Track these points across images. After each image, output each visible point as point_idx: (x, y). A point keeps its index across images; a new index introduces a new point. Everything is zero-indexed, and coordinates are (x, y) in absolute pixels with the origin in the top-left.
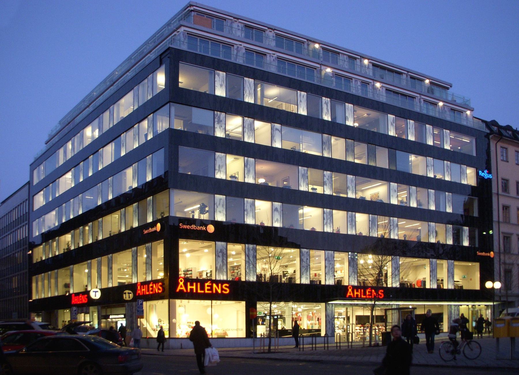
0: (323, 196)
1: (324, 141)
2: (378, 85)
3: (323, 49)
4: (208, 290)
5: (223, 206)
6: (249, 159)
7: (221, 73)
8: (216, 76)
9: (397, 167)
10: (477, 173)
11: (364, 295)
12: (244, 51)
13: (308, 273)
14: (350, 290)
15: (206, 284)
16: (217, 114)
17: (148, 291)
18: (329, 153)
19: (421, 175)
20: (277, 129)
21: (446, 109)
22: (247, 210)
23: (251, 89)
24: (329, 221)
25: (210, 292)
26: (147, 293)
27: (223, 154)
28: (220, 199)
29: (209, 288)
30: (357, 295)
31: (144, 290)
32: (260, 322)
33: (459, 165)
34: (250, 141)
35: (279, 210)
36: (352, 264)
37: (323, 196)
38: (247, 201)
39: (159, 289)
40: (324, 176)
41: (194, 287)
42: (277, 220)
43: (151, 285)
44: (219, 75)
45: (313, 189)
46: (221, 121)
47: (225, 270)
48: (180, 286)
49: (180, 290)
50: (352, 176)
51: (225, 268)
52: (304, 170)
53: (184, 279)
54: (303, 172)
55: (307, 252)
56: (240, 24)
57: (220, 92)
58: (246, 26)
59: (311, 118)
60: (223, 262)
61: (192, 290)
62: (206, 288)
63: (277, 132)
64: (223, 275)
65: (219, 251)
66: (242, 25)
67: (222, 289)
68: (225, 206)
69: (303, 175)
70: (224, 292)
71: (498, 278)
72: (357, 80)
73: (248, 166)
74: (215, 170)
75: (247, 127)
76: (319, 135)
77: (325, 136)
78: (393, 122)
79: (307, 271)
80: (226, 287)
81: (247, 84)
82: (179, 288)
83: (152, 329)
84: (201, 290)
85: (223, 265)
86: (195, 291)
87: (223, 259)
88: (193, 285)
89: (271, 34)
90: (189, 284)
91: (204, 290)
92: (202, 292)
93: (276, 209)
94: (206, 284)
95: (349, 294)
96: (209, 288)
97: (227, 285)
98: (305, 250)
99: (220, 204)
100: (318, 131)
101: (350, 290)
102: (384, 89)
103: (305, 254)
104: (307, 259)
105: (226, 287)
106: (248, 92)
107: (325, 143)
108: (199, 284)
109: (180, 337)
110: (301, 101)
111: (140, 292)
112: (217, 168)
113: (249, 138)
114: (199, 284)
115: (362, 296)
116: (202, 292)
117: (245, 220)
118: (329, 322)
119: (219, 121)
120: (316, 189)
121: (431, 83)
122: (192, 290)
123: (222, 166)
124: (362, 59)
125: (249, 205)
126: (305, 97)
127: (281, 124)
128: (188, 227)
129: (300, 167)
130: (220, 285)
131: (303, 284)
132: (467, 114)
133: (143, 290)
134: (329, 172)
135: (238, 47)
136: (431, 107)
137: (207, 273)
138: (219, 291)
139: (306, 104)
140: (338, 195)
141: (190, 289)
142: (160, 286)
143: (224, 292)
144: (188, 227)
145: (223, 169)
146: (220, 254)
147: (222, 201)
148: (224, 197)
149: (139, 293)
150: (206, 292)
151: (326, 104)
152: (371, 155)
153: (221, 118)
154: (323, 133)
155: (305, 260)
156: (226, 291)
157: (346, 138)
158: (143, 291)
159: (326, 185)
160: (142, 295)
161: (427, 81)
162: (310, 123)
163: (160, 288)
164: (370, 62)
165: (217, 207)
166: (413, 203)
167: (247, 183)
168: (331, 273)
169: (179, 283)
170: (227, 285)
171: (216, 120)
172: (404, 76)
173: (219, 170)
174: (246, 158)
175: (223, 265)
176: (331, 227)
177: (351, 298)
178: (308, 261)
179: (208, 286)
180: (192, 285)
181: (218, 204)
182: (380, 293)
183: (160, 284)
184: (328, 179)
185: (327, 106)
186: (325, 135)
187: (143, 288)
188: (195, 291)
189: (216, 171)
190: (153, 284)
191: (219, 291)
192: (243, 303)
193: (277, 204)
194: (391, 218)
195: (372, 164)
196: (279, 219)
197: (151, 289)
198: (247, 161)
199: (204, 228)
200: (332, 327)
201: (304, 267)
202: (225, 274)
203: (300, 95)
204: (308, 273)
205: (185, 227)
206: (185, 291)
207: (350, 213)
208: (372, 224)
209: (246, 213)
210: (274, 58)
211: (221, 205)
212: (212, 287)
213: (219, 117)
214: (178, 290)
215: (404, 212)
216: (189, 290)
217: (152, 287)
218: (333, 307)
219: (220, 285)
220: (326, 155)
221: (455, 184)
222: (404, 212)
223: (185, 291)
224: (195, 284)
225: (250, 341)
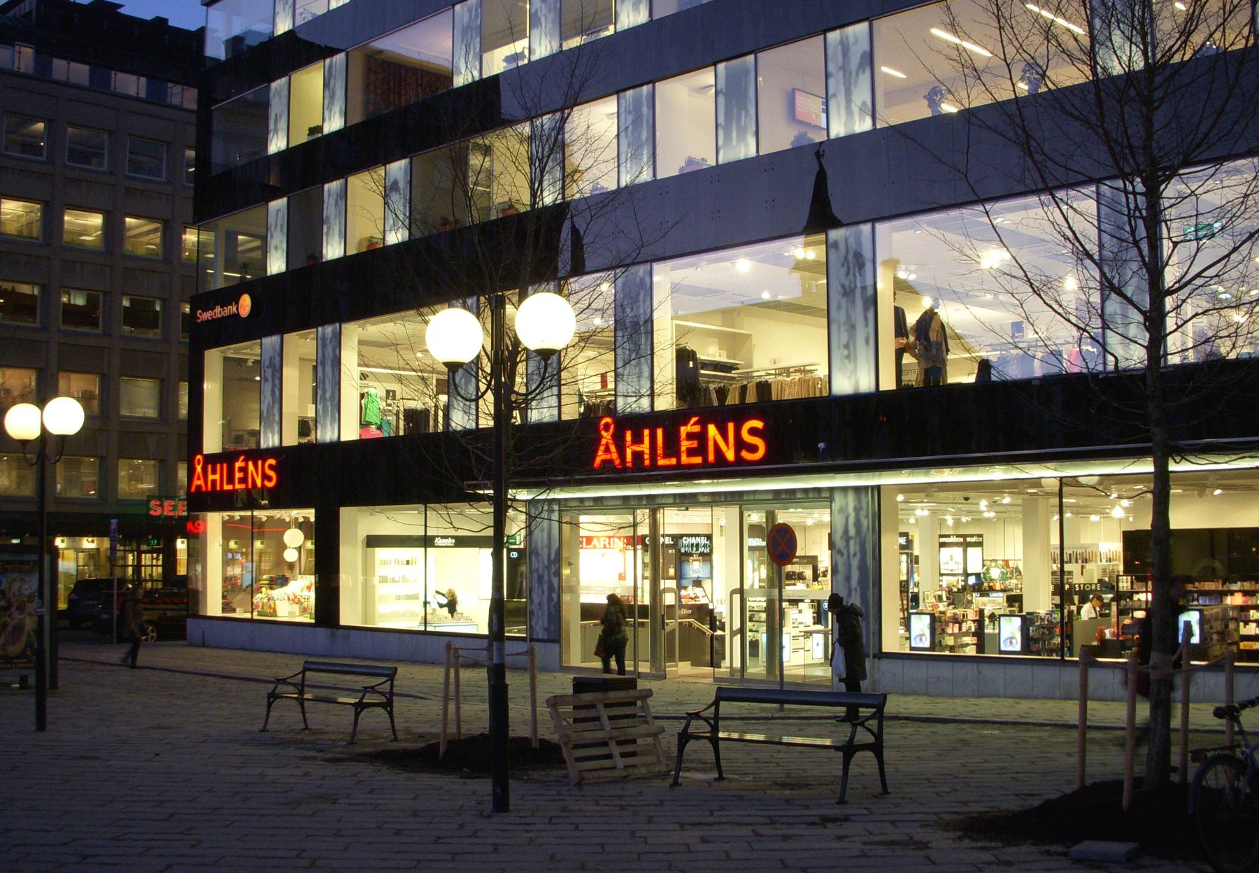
4: (691, 452)
14: (607, 436)
17: (231, 480)
25: (698, 460)
26: (227, 487)
29: (694, 444)
31: (217, 477)
35: (401, 185)
39: (265, 477)
43: (238, 464)
49: (603, 461)
62: (685, 445)
67: (740, 445)
70: (746, 455)
80: (753, 432)
83: (904, 586)
93: (394, 187)
95: (601, 456)
96: (694, 444)
97: (758, 424)
101: (607, 436)
105: (753, 432)
108: (660, 432)
111: (201, 482)
114: (660, 432)
116: (674, 461)
130: (731, 427)
133: (211, 477)
137: (744, 389)
140: (593, 38)
142: (271, 467)
143: (746, 455)
147: (280, 214)
149: (199, 487)
150: (685, 459)
156: (753, 449)
158: (214, 482)
160: (207, 493)
163: (272, 473)
170: (758, 424)
179: (690, 436)
182: (746, 437)
183: (272, 461)
187: (214, 472)
190: (246, 461)
192: (342, 509)
197: (238, 475)
200: (550, 599)
208: (734, 102)
216: (629, 457)
217: (244, 470)
225: (322, 632)
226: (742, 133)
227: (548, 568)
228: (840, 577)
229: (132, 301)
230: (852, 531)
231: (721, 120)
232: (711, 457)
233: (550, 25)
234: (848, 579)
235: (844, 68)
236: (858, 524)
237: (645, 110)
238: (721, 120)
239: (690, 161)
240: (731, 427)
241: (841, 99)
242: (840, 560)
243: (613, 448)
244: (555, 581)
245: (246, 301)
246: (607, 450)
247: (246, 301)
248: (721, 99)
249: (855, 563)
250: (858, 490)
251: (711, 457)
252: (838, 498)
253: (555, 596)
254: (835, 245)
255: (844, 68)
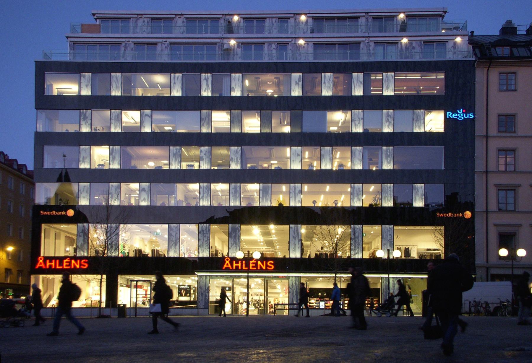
0: (200, 171)
1: (203, 117)
2: (301, 42)
3: (244, 18)
5: (87, 192)
6: (115, 147)
7: (86, 74)
8: (82, 78)
9: (303, 128)
10: (445, 115)
11: (59, 266)
12: (132, 46)
13: (178, 247)
14: (227, 262)
16: (83, 112)
20: (146, 115)
21: (414, 45)
22: (111, 193)
23: (118, 83)
24: (205, 195)
27: (87, 147)
28: (84, 186)
29: (254, 265)
30: (237, 267)
32: (183, 294)
33: (412, 111)
34: (116, 131)
35: (147, 189)
36: (233, 235)
37: (200, 171)
38: (112, 186)
42: (144, 199)
44: (84, 76)
45: (189, 166)
46: (87, 118)
47: (86, 248)
50: (236, 147)
51: (86, 246)
52: (176, 149)
53: (44, 257)
54: (175, 151)
55: (176, 227)
56: (146, 20)
58: (153, 19)
60: (84, 240)
61: (51, 266)
62: (65, 264)
63: (147, 118)
64: (83, 251)
65: (80, 231)
66: (148, 19)
67: (81, 265)
68: (89, 192)
70: (268, 268)
72: (270, 44)
73: (114, 154)
74: (79, 161)
75: (113, 118)
79: (176, 245)
80: (270, 263)
81: (115, 79)
82: (39, 265)
84: (59, 266)
85: (84, 243)
86: (53, 267)
87: (84, 238)
89: (180, 21)
90: (234, 262)
91: (62, 265)
92: (61, 267)
94: (65, 261)
96: (254, 265)
97: (272, 262)
98: (175, 225)
99: (84, 191)
100: (194, 109)
101: (227, 262)
102: (311, 44)
103: (174, 228)
104: (176, 233)
105: (270, 263)
106: (114, 86)
109: (231, 310)
110: (175, 83)
112: (81, 159)
113: (115, 128)
114: (58, 261)
115: (244, 268)
116: (61, 267)
117: (110, 202)
118: (202, 294)
119: (85, 118)
120: (193, 166)
121: (407, 16)
122: (51, 266)
123: (86, 158)
124: (298, 16)
125: (114, 189)
126: (180, 78)
127: (151, 109)
128: (49, 213)
130: (265, 262)
131: (171, 258)
132: (455, 43)
134: (206, 148)
135: (126, 44)
136: (391, 49)
138: (78, 266)
141: (236, 266)
143: (268, 268)
144: (49, 213)
145: (87, 160)
146: (82, 234)
148: (89, 184)
150: (65, 267)
151: (206, 79)
153: (87, 115)
155: (174, 234)
156: (271, 267)
157: (231, 110)
159: (203, 160)
161: (402, 16)
162: (191, 102)
164: (308, 17)
165: (81, 193)
166: (326, 165)
168: (205, 245)
169: (225, 262)
170: (272, 262)
171: (82, 117)
172: (362, 20)
173: (84, 162)
174: (111, 147)
175: (84, 243)
176: (208, 200)
177: (228, 270)
178: (178, 235)
179: (66, 262)
180: (51, 262)
181: (82, 191)
188: (53, 267)
189: (81, 163)
191: (78, 266)
193: (145, 185)
194: (292, 185)
196: (146, 198)
198: (113, 149)
199: (64, 213)
200: (205, 299)
201: (172, 241)
202: (86, 251)
204: (178, 247)
205: (46, 213)
206: (231, 268)
207: (233, 184)
208: (264, 193)
209: (110, 196)
210: (166, 45)
211: (85, 191)
212: (70, 263)
213: (85, 115)
214: (37, 267)
216: (234, 268)
218: (208, 280)
220: (204, 130)
221: (402, 135)
223: (231, 268)
224: (54, 261)
226: (267, 200)
227: (205, 291)
228: (291, 294)
229: (501, 247)
230: (294, 284)
231: (261, 196)
232: (259, 268)
233: (207, 161)
234: (293, 294)
235: (295, 192)
236: (295, 283)
237: (238, 189)
238: (261, 196)
240: (265, 262)
241: (294, 198)
242: (291, 290)
243: (229, 264)
244: (207, 294)
246: (227, 264)
248: (261, 192)
249: (295, 291)
250: (295, 277)
251: (259, 268)
252: (291, 278)
253: (207, 298)
254: (292, 228)
255: (295, 192)
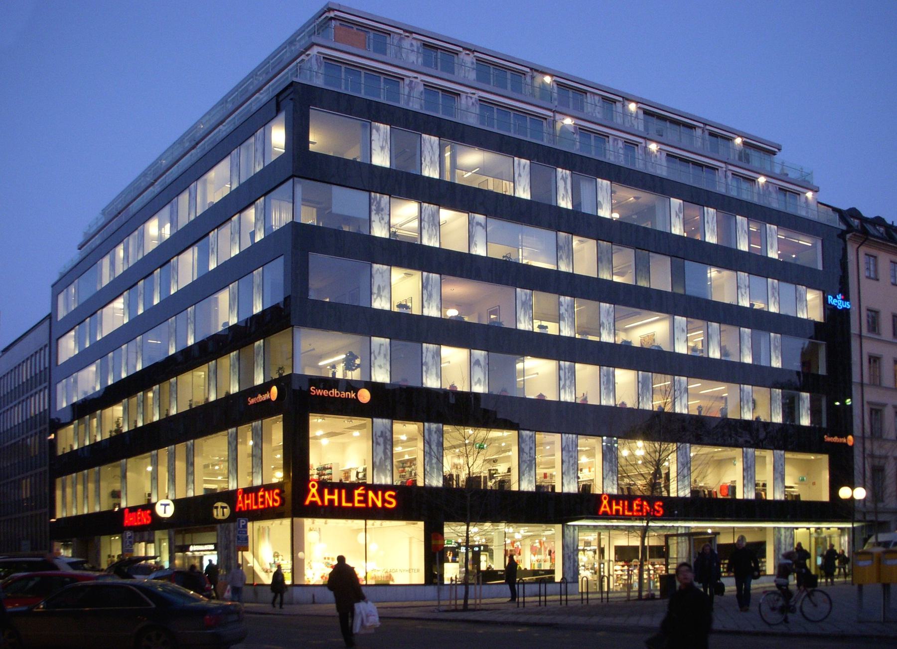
0: (558, 339)
1: (561, 243)
2: (653, 147)
3: (559, 84)
4: (359, 502)
5: (385, 356)
6: (431, 275)
7: (382, 125)
8: (374, 131)
9: (687, 288)
10: (825, 300)
11: (629, 511)
12: (422, 88)
13: (533, 473)
14: (605, 502)
15: (357, 492)
16: (376, 198)
17: (256, 503)
18: (568, 265)
19: (728, 302)
20: (478, 224)
21: (770, 189)
22: (426, 364)
23: (434, 154)
24: (568, 382)
25: (363, 505)
26: (255, 507)
27: (385, 267)
28: (381, 345)
29: (361, 498)
30: (617, 511)
31: (249, 501)
32: (450, 558)
33: (794, 286)
34: (431, 245)
35: (482, 363)
36: (608, 457)
37: (558, 339)
38: (427, 349)
39: (274, 500)
40: (560, 304)
41: (336, 497)
42: (479, 381)
43: (261, 493)
44: (378, 130)
45: (540, 327)
46: (382, 210)
47: (389, 467)
48: (311, 494)
49: (311, 502)
50: (608, 305)
51: (388, 463)
52: (526, 294)
53: (319, 482)
54: (524, 298)
55: (531, 437)
56: (414, 42)
57: (381, 159)
58: (426, 45)
59: (538, 204)
60: (385, 453)
61: (331, 501)
62: (357, 498)
63: (479, 229)
64: (386, 476)
65: (379, 434)
66: (419, 43)
67: (384, 501)
68: (388, 357)
69: (524, 304)
70: (387, 505)
71: (861, 482)
72: (616, 138)
73: (429, 288)
74: (371, 294)
75: (426, 219)
76: (552, 234)
77: (562, 235)
78: (680, 212)
79: (530, 470)
80: (390, 496)
81: (428, 145)
82: (310, 498)
84: (347, 502)
85: (386, 459)
86: (336, 504)
87: (385, 448)
88: (333, 494)
89: (469, 59)
90: (326, 491)
91: (353, 502)
92: (350, 505)
94: (357, 492)
95: (602, 509)
96: (361, 498)
97: (393, 493)
98: (528, 432)
99: (379, 353)
100: (549, 227)
101: (605, 502)
102: (664, 154)
103: (527, 439)
104: (531, 448)
105: (390, 496)
106: (428, 159)
107: (561, 247)
108: (343, 492)
109: (312, 583)
110: (520, 175)
111: (241, 505)
112: (375, 290)
113: (430, 238)
114: (343, 492)
115: (626, 513)
116: (350, 505)
117: (424, 381)
118: (569, 557)
119: (379, 210)
120: (546, 327)
121: (744, 143)
122: (331, 501)
123: (384, 288)
124: (626, 102)
125: (430, 355)
126: (527, 168)
127: (486, 214)
128: (325, 393)
129: (518, 290)
130: (380, 493)
131: (523, 492)
132: (806, 198)
133: (246, 502)
134: (568, 298)
135: (411, 82)
136: (745, 185)
137: (358, 473)
138: (379, 504)
139: (528, 180)
141: (329, 500)
142: (277, 494)
143: (387, 505)
144: (325, 393)
145: (385, 293)
146: (381, 440)
148: (388, 340)
149: (240, 508)
150: (357, 505)
151: (564, 179)
152: (642, 268)
153: (383, 205)
154: (558, 229)
155: (527, 449)
156: (390, 503)
157: (597, 239)
158: (248, 504)
159: (564, 320)
160: (245, 511)
161: (738, 141)
162: (535, 214)
164: (639, 108)
165: (375, 358)
166: (714, 352)
167: (428, 317)
168: (571, 472)
169: (310, 490)
170: (393, 493)
171: (373, 207)
172: (699, 132)
173: (379, 295)
174: (425, 274)
175: (386, 459)
176: (571, 392)
177: (606, 516)
178: (533, 451)
179: (359, 495)
180: (331, 493)
181: (376, 353)
182: (657, 507)
183: (277, 491)
184: (566, 310)
185: (565, 183)
186: (561, 233)
187: (248, 499)
188: (336, 504)
189: (374, 297)
190: (264, 491)
191: (379, 504)
192: (421, 525)
193: (479, 354)
194: (676, 377)
195: (643, 283)
196: (482, 380)
197: (260, 500)
198: (428, 278)
199: (353, 395)
200: (574, 566)
201: (525, 462)
202: (389, 474)
203: (519, 164)
204: (533, 473)
205: (319, 392)
206: (320, 503)
207: (605, 368)
208: (643, 388)
209: (424, 368)
210: (473, 100)
211: (382, 355)
212: (366, 496)
213: (379, 203)
214: (307, 502)
215: (698, 367)
216: (326, 503)
217: (263, 496)
218: (576, 532)
219: (380, 493)
220: (563, 268)
221: (787, 318)
222: (698, 367)
223: (320, 503)
224: (336, 491)
225: (432, 589)
239: (541, 395)
245: (274, 389)
247: (274, 389)
